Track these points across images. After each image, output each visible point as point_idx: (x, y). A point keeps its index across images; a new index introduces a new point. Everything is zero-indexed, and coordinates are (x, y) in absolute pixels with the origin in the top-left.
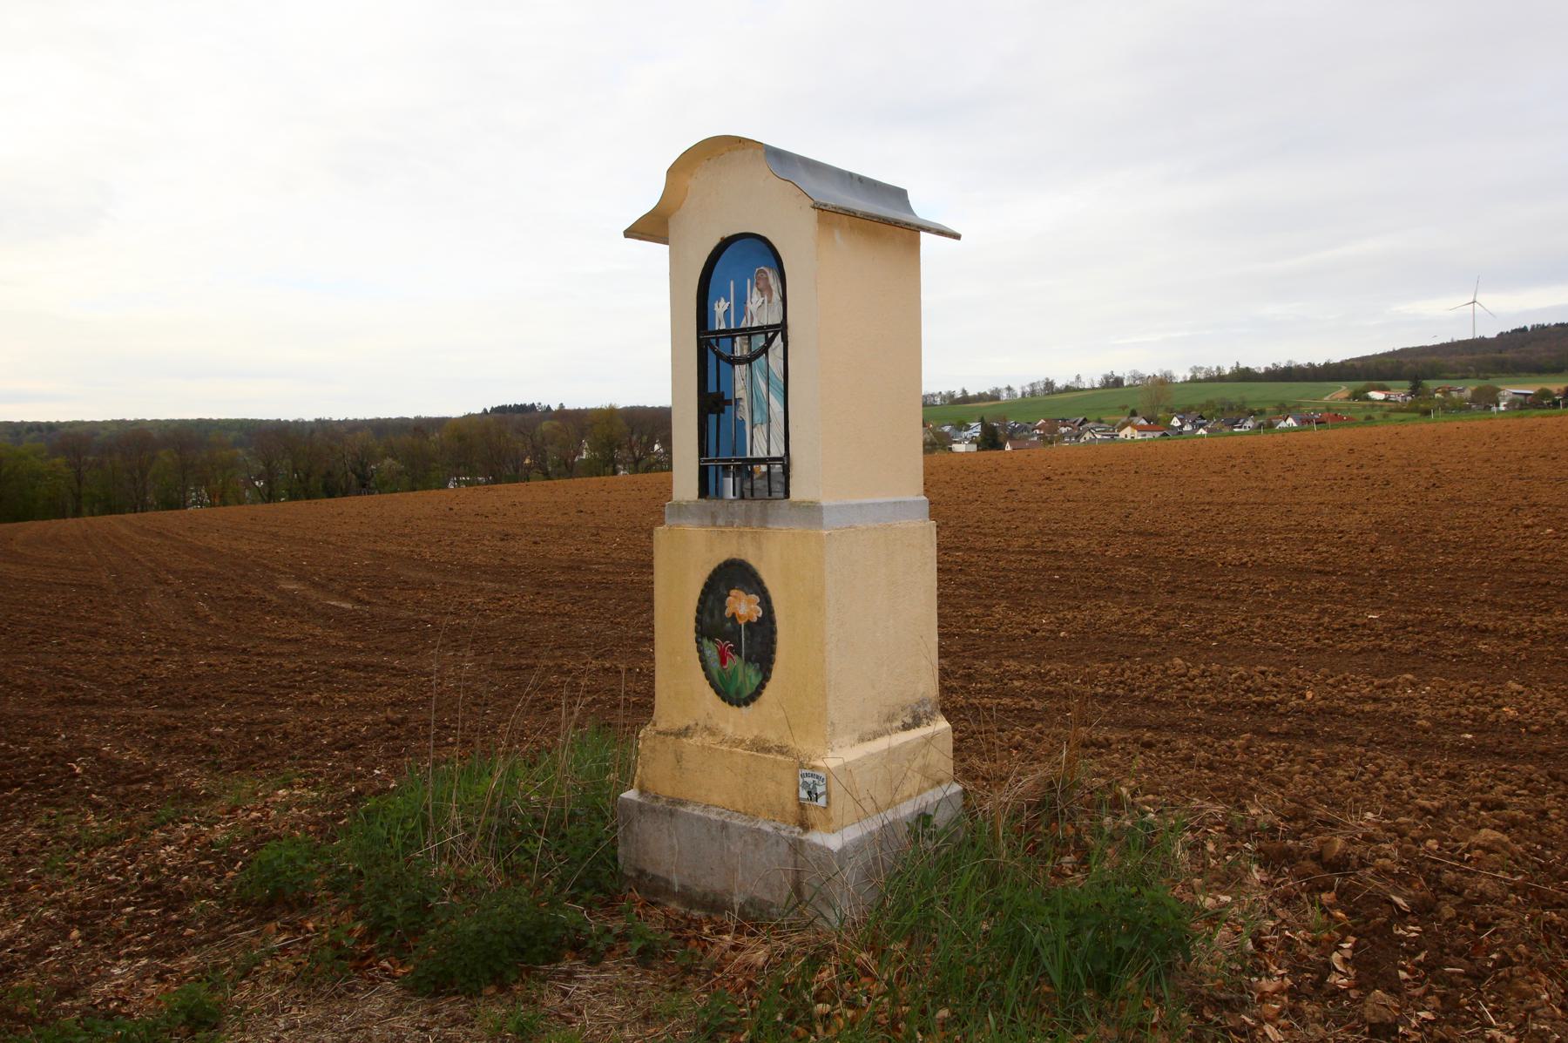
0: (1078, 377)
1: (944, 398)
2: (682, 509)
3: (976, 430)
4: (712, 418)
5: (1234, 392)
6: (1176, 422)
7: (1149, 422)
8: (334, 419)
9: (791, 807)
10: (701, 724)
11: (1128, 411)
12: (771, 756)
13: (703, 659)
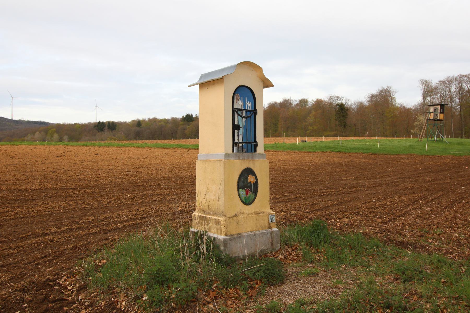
4: (236, 131)
9: (267, 225)
10: (239, 212)
13: (239, 195)
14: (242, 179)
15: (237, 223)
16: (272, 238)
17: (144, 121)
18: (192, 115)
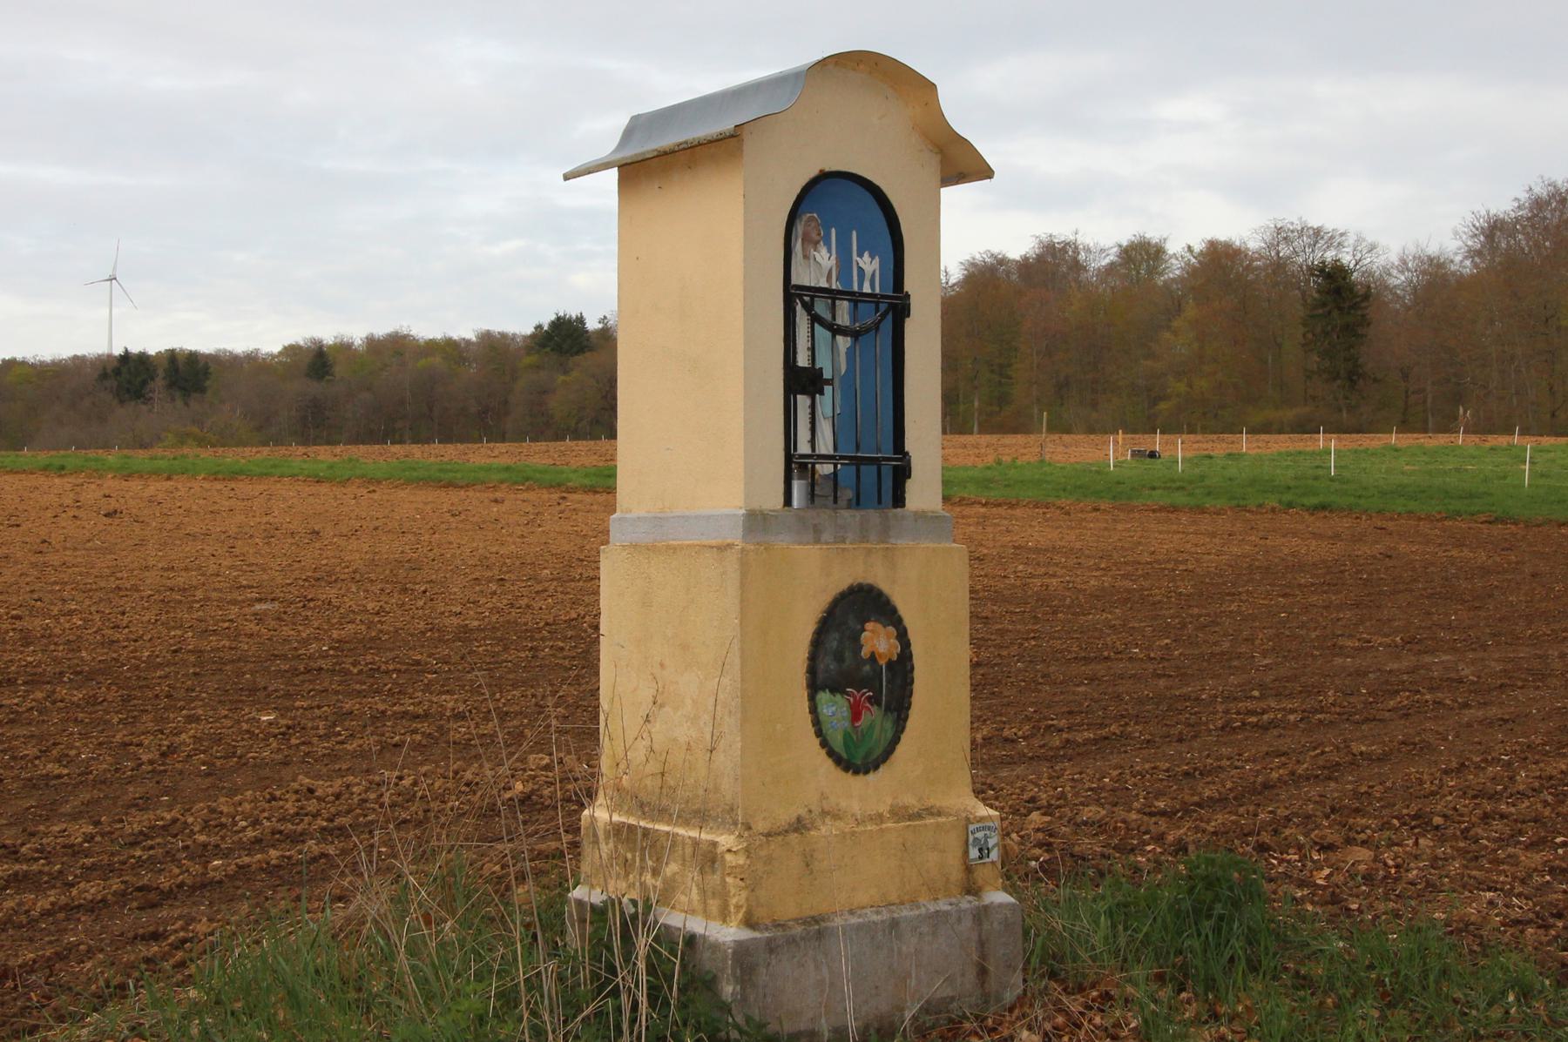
4: (803, 401)
8: (163, 351)
9: (956, 874)
10: (816, 810)
14: (833, 642)
15: (808, 865)
16: (982, 944)
17: (344, 348)
18: (581, 320)
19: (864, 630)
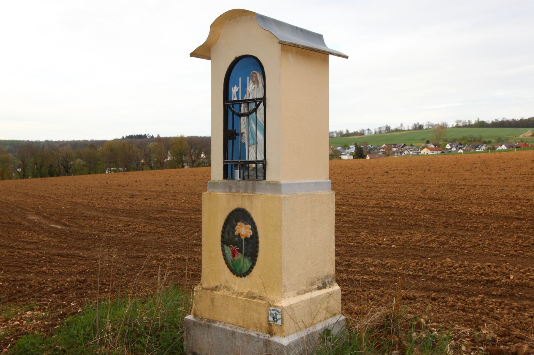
0: (402, 125)
1: (337, 134)
2: (215, 184)
3: (353, 149)
4: (230, 142)
5: (477, 133)
6: (448, 146)
7: (435, 146)
9: (265, 325)
11: (425, 141)
12: (255, 301)
15: (212, 302)
19: (237, 225)
